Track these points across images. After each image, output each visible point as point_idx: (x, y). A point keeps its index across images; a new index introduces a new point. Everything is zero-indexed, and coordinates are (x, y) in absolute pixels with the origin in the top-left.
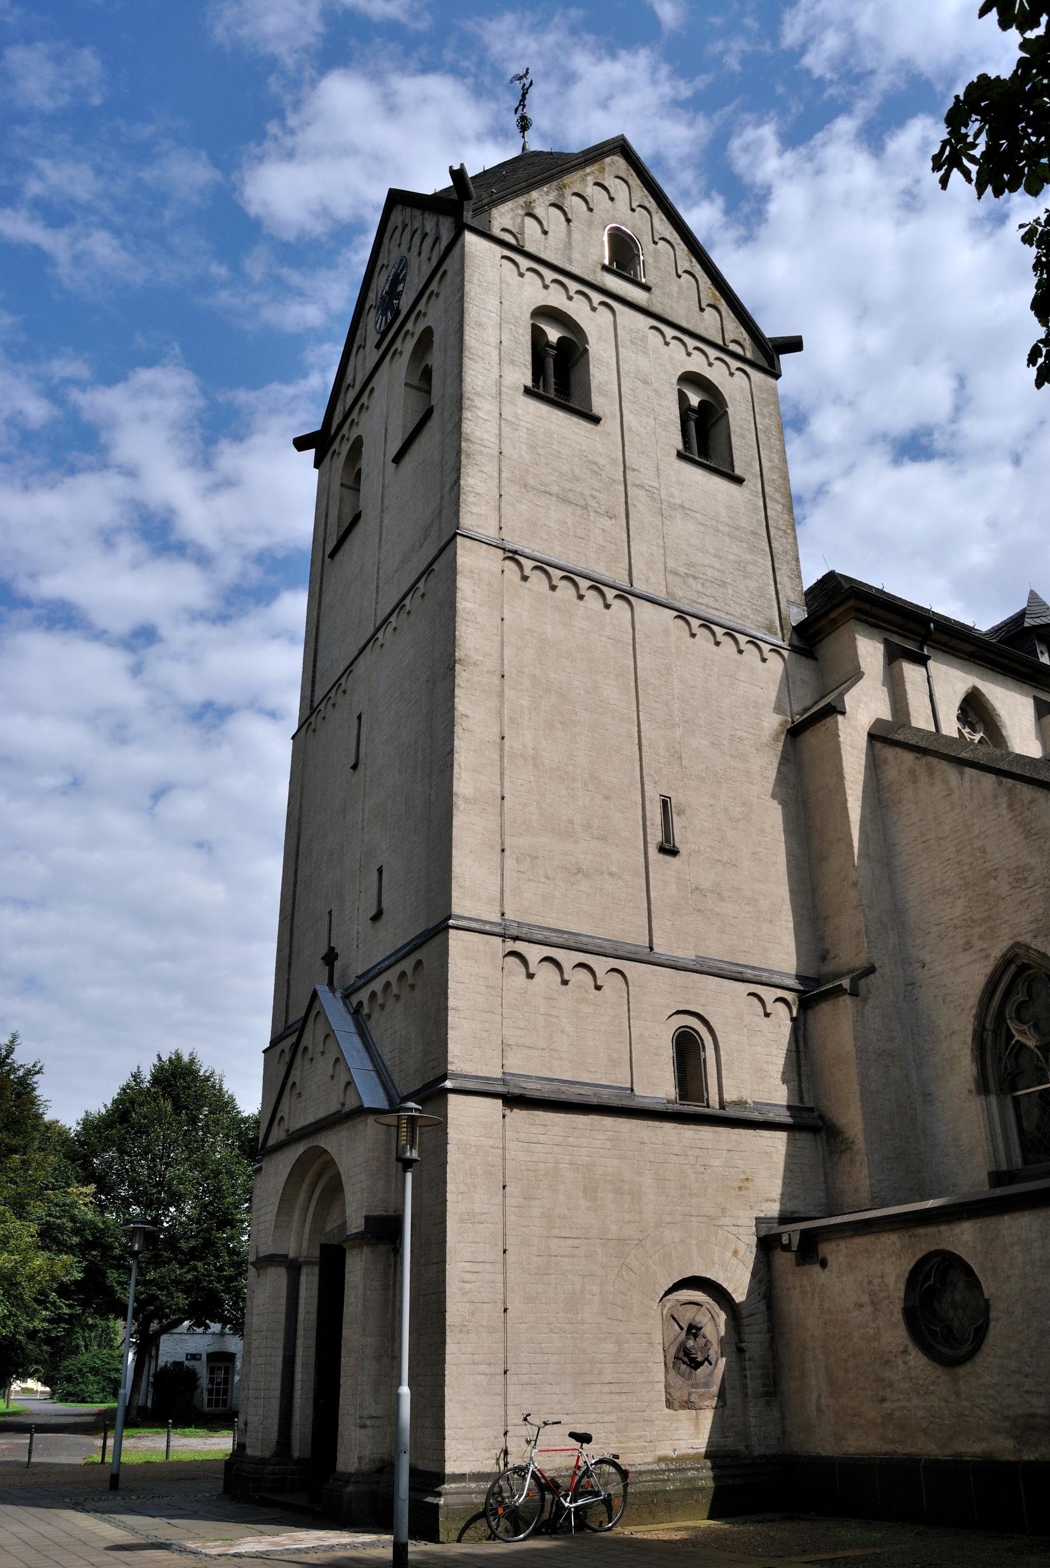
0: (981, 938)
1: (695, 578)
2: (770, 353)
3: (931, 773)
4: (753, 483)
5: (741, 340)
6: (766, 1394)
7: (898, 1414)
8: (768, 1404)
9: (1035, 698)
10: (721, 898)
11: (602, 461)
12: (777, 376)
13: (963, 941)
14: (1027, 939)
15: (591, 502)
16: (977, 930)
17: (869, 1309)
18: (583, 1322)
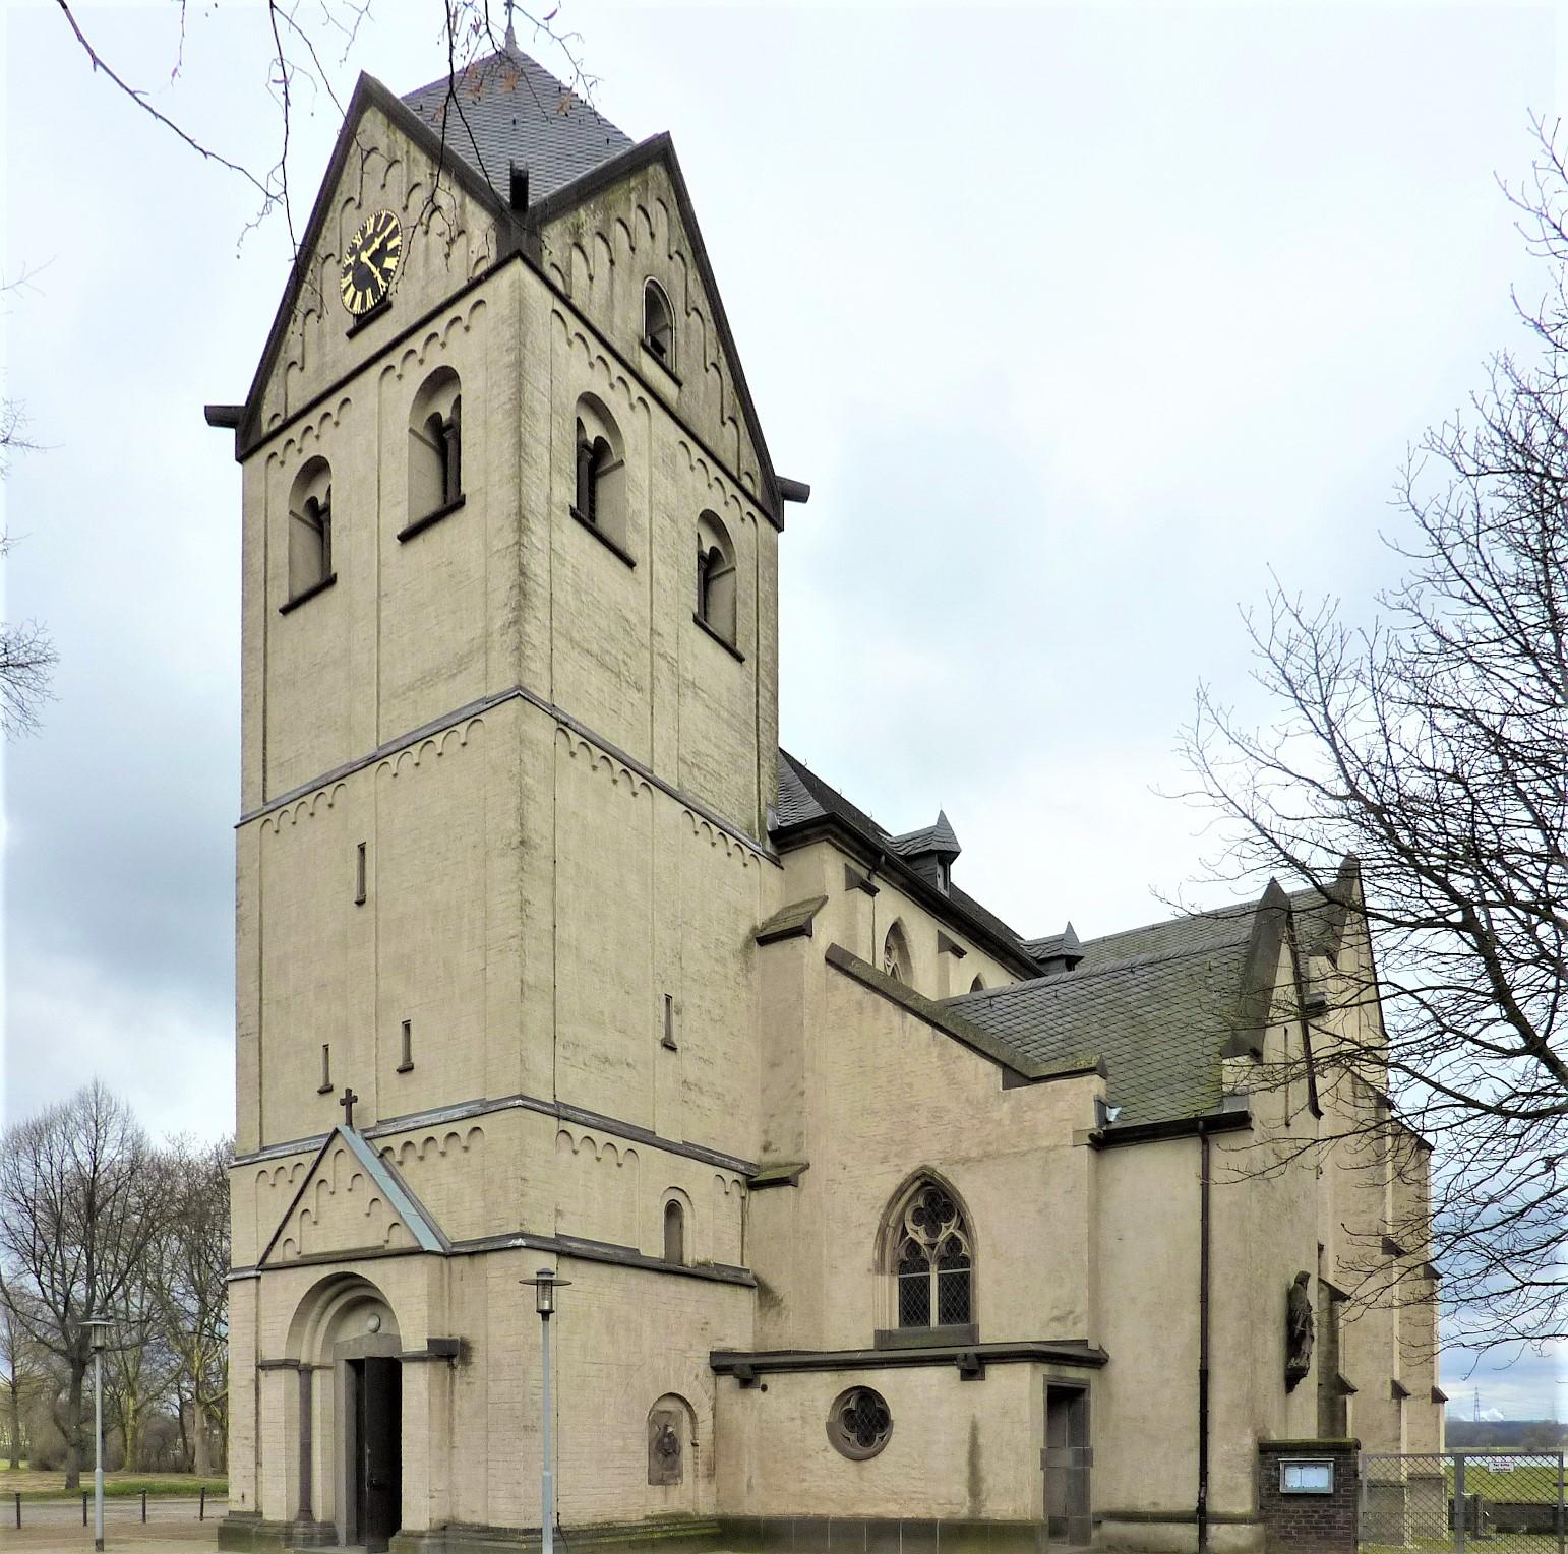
0: (896, 1155)
1: (699, 769)
2: (775, 496)
3: (877, 1009)
4: (750, 663)
5: (753, 473)
6: (709, 1475)
7: (814, 1490)
8: (709, 1482)
9: (847, 868)
10: (700, 1090)
11: (633, 618)
12: (779, 528)
13: (881, 1155)
14: (933, 1164)
15: (624, 669)
16: (894, 1149)
17: (799, 1422)
18: (603, 1424)
